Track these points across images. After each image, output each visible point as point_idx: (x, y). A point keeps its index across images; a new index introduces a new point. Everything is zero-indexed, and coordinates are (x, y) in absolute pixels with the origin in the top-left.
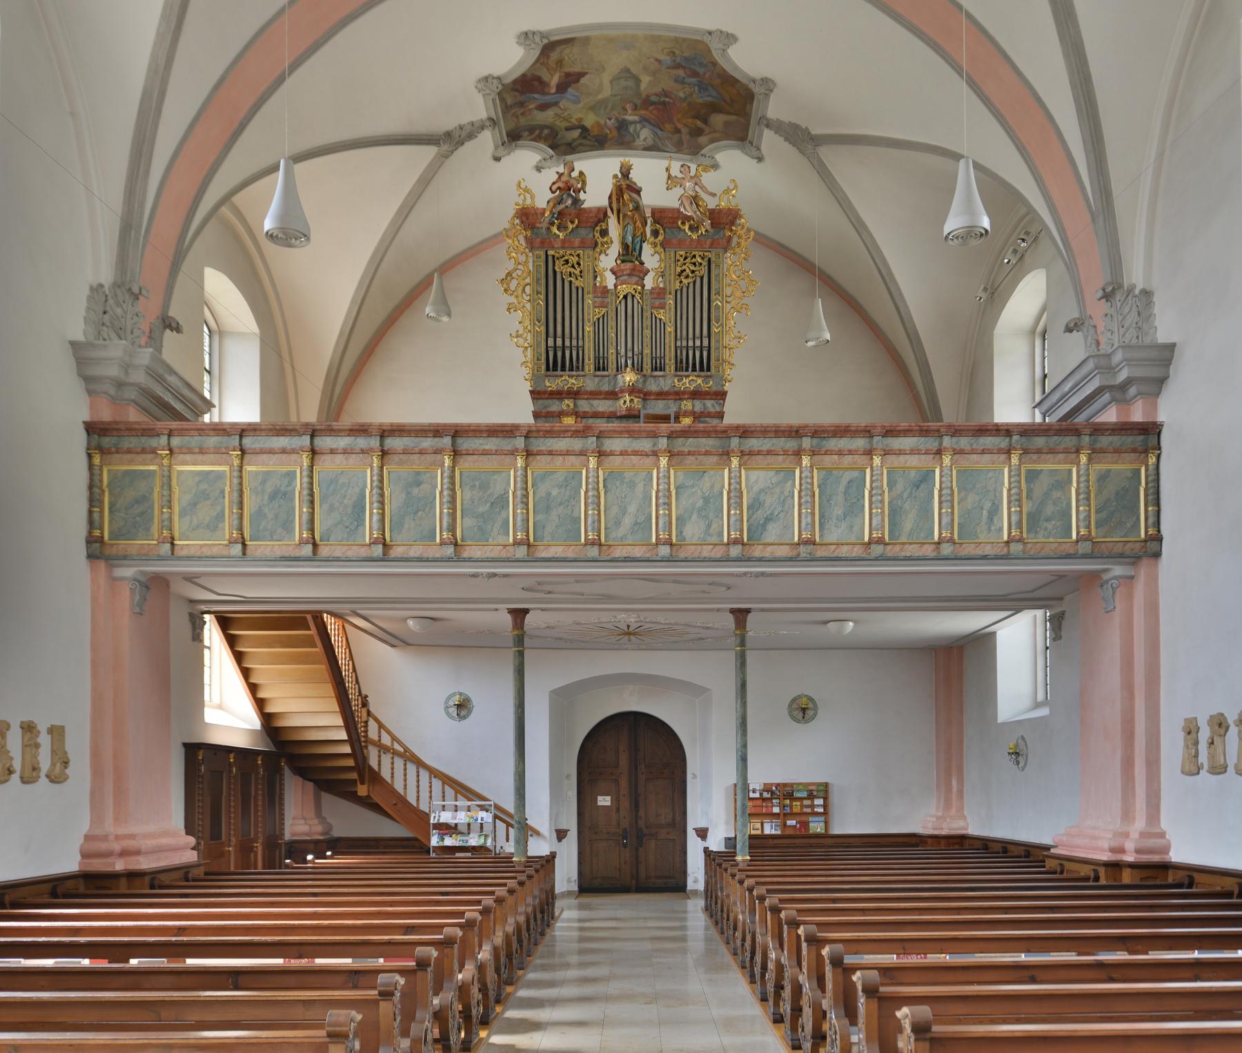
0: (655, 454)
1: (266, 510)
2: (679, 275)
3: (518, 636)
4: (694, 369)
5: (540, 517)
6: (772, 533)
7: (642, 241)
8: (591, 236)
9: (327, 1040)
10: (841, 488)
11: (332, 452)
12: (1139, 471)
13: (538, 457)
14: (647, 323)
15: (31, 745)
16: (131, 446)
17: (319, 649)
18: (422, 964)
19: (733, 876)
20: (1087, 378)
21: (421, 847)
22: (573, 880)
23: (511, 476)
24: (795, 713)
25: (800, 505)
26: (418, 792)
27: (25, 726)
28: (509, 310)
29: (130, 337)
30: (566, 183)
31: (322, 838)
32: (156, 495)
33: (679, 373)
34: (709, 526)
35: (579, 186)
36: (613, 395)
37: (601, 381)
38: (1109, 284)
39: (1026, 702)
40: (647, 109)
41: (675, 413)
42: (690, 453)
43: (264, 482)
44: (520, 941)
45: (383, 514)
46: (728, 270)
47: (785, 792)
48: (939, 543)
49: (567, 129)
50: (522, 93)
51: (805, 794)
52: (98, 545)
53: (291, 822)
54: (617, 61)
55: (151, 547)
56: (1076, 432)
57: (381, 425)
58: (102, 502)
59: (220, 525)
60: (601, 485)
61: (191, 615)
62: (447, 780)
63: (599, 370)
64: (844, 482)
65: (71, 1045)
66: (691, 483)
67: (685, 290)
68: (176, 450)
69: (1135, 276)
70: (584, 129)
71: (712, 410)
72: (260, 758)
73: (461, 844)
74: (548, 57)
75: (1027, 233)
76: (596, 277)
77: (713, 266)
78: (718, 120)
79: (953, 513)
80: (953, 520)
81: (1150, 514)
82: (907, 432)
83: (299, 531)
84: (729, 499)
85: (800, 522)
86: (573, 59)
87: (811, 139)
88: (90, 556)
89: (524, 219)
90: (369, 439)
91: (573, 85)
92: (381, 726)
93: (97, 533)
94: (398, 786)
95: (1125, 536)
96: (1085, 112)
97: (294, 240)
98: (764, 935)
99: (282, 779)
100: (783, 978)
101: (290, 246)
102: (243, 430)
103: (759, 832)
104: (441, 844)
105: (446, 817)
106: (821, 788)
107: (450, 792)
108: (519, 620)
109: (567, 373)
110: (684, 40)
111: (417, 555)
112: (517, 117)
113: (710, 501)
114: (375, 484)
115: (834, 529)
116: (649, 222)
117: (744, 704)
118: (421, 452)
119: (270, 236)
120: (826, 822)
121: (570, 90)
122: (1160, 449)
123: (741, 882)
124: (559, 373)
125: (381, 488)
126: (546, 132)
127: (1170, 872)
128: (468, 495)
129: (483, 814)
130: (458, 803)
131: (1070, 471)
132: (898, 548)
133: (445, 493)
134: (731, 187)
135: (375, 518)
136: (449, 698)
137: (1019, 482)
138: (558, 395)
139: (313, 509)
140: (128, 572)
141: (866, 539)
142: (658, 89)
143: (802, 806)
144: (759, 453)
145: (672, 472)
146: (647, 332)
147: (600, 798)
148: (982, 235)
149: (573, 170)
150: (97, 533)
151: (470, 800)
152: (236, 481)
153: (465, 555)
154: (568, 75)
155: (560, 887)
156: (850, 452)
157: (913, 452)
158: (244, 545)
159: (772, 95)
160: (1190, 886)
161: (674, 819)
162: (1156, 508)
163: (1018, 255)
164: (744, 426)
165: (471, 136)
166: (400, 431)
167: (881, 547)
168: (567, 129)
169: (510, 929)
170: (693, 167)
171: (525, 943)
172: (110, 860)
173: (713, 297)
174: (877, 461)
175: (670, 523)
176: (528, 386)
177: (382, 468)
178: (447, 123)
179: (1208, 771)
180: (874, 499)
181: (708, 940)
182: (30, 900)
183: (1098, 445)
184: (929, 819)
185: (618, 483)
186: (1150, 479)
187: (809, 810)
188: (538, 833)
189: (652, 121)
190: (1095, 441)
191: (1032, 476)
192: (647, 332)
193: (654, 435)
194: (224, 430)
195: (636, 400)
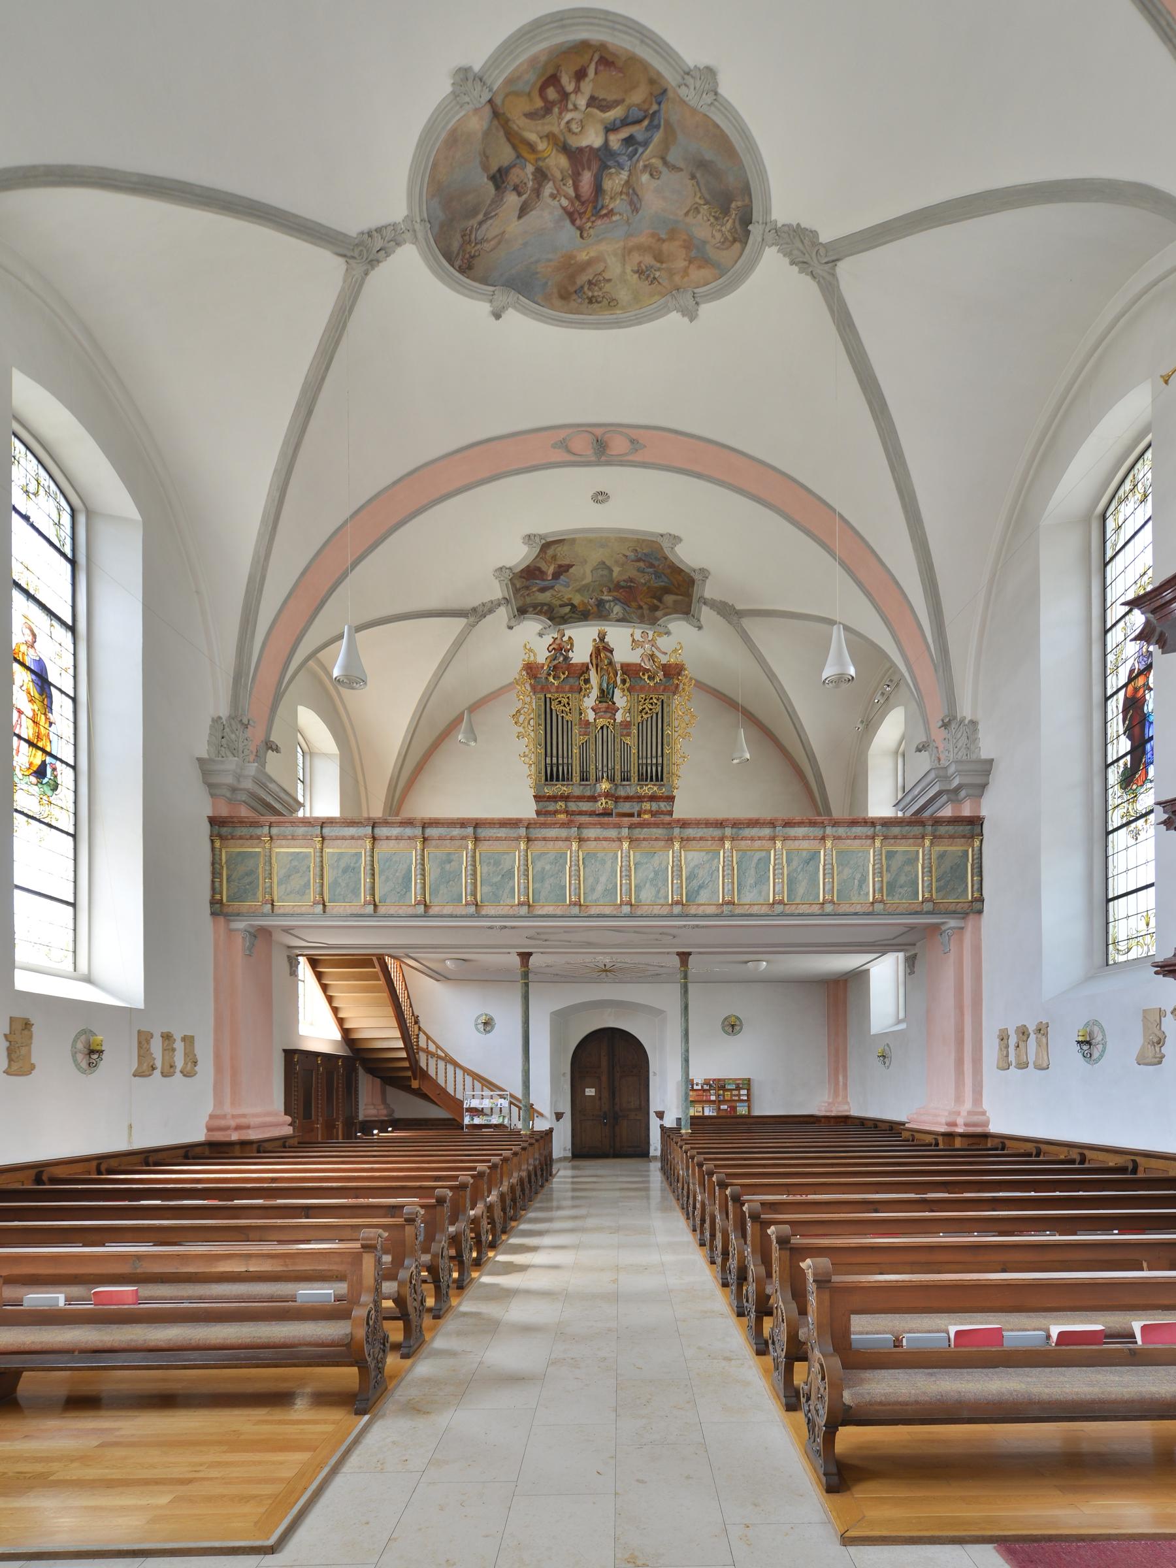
0: (620, 840)
1: (340, 880)
2: (641, 712)
3: (524, 971)
4: (651, 780)
5: (537, 885)
6: (703, 897)
7: (614, 687)
8: (577, 683)
9: (362, 1250)
10: (753, 864)
11: (388, 838)
12: (967, 851)
13: (536, 842)
14: (618, 746)
15: (169, 1049)
16: (243, 834)
17: (382, 982)
18: (441, 1201)
19: (677, 1143)
20: (930, 785)
21: (454, 1124)
22: (568, 1148)
23: (516, 855)
24: (726, 1028)
25: (723, 877)
26: (455, 1085)
27: (165, 1036)
28: (518, 737)
29: (242, 755)
30: (559, 645)
31: (386, 1118)
32: (260, 870)
33: (640, 783)
34: (658, 892)
35: (569, 647)
36: (593, 799)
37: (584, 788)
38: (946, 716)
39: (891, 1020)
40: (618, 592)
41: (638, 811)
42: (644, 839)
43: (338, 860)
44: (523, 1190)
45: (424, 884)
46: (676, 708)
47: (720, 1085)
48: (823, 904)
49: (561, 606)
50: (527, 580)
51: (733, 1087)
52: (218, 905)
53: (364, 1107)
54: (595, 556)
55: (257, 907)
56: (922, 823)
57: (423, 819)
58: (221, 874)
59: (307, 891)
60: (581, 862)
61: (289, 957)
62: (476, 1077)
63: (583, 780)
64: (755, 860)
65: (178, 1255)
66: (645, 861)
67: (645, 722)
68: (275, 837)
69: (966, 711)
70: (573, 606)
71: (664, 809)
72: (340, 1061)
73: (486, 1122)
74: (546, 553)
75: (891, 681)
76: (581, 714)
77: (665, 705)
78: (669, 599)
79: (833, 882)
80: (833, 887)
81: (975, 882)
82: (800, 824)
83: (364, 896)
84: (672, 873)
85: (723, 888)
86: (564, 555)
87: (736, 613)
88: (213, 914)
89: (529, 671)
90: (414, 830)
91: (564, 574)
92: (428, 1038)
93: (218, 897)
94: (441, 1081)
95: (957, 898)
96: (929, 592)
97: (355, 684)
98: (694, 1184)
99: (357, 1076)
100: (705, 1214)
101: (353, 688)
102: (323, 823)
103: (701, 1114)
104: (471, 1122)
105: (475, 1103)
106: (746, 1082)
107: (478, 1085)
108: (525, 961)
109: (561, 783)
110: (644, 541)
111: (449, 913)
112: (524, 597)
113: (660, 873)
114: (418, 862)
115: (748, 893)
116: (619, 673)
117: (687, 1021)
118: (452, 839)
119: (338, 680)
120: (749, 1107)
121: (562, 577)
122: (982, 835)
123: (681, 1147)
124: (554, 782)
125: (423, 865)
126: (545, 608)
127: (989, 1140)
128: (485, 869)
129: (502, 1101)
130: (483, 1093)
131: (918, 852)
132: (793, 907)
133: (469, 868)
134: (678, 648)
135: (419, 886)
136: (478, 1018)
137: (881, 859)
138: (554, 798)
139: (374, 879)
140: (240, 925)
141: (771, 901)
142: (625, 577)
143: (732, 1095)
144: (694, 839)
145: (632, 852)
146: (618, 753)
147: (587, 1090)
148: (849, 680)
149: (564, 635)
150: (218, 897)
151: (492, 1091)
152: (318, 860)
153: (483, 913)
154: (560, 566)
155: (556, 1154)
156: (760, 838)
157: (804, 838)
158: (324, 905)
159: (708, 581)
160: (1003, 1149)
161: (640, 1105)
162: (979, 878)
163: (885, 697)
164: (683, 820)
165: (491, 611)
166: (436, 823)
167: (782, 906)
168: (561, 606)
169: (514, 1180)
170: (651, 633)
171: (527, 1191)
172: (228, 1132)
173: (665, 728)
174: (779, 844)
175: (631, 889)
176: (532, 792)
177: (423, 850)
178: (475, 602)
179: (1015, 1067)
180: (776, 872)
181: (662, 1190)
182: (168, 1161)
183: (938, 833)
184: (823, 1104)
185: (593, 861)
186: (975, 857)
187: (737, 1098)
188: (541, 1115)
189: (622, 601)
190: (936, 830)
191: (890, 855)
192: (618, 753)
193: (618, 826)
194: (310, 822)
195: (609, 802)
